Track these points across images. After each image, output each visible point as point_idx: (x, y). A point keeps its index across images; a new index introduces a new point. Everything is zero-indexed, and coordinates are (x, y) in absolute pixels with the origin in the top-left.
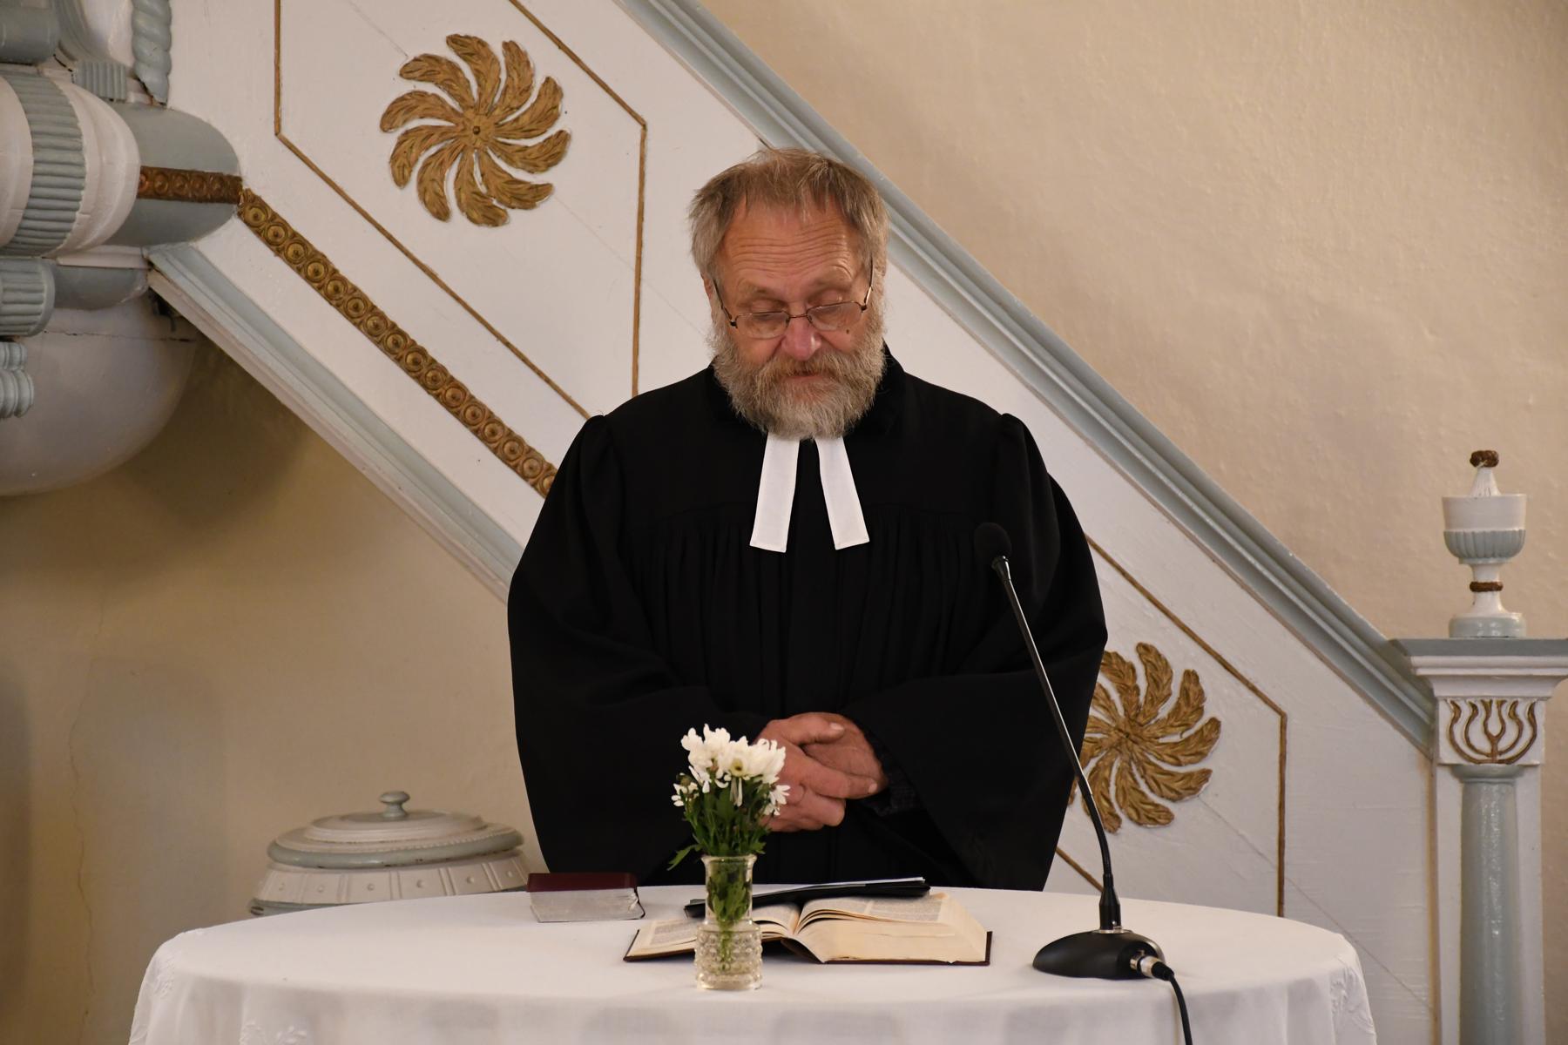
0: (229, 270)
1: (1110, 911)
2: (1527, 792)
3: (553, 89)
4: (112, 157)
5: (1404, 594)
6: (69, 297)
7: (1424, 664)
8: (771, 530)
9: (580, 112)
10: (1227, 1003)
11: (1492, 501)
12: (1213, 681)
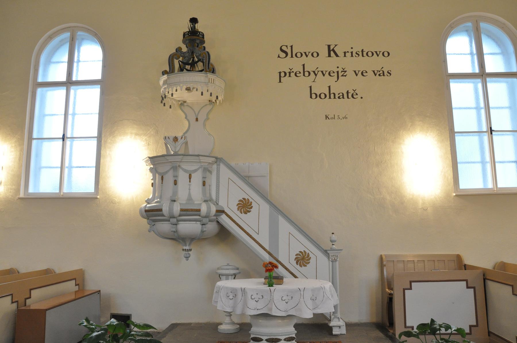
0: (223, 218)
2: (337, 262)
4: (214, 209)
5: (327, 245)
6: (210, 221)
7: (328, 252)
11: (334, 237)
12: (310, 253)
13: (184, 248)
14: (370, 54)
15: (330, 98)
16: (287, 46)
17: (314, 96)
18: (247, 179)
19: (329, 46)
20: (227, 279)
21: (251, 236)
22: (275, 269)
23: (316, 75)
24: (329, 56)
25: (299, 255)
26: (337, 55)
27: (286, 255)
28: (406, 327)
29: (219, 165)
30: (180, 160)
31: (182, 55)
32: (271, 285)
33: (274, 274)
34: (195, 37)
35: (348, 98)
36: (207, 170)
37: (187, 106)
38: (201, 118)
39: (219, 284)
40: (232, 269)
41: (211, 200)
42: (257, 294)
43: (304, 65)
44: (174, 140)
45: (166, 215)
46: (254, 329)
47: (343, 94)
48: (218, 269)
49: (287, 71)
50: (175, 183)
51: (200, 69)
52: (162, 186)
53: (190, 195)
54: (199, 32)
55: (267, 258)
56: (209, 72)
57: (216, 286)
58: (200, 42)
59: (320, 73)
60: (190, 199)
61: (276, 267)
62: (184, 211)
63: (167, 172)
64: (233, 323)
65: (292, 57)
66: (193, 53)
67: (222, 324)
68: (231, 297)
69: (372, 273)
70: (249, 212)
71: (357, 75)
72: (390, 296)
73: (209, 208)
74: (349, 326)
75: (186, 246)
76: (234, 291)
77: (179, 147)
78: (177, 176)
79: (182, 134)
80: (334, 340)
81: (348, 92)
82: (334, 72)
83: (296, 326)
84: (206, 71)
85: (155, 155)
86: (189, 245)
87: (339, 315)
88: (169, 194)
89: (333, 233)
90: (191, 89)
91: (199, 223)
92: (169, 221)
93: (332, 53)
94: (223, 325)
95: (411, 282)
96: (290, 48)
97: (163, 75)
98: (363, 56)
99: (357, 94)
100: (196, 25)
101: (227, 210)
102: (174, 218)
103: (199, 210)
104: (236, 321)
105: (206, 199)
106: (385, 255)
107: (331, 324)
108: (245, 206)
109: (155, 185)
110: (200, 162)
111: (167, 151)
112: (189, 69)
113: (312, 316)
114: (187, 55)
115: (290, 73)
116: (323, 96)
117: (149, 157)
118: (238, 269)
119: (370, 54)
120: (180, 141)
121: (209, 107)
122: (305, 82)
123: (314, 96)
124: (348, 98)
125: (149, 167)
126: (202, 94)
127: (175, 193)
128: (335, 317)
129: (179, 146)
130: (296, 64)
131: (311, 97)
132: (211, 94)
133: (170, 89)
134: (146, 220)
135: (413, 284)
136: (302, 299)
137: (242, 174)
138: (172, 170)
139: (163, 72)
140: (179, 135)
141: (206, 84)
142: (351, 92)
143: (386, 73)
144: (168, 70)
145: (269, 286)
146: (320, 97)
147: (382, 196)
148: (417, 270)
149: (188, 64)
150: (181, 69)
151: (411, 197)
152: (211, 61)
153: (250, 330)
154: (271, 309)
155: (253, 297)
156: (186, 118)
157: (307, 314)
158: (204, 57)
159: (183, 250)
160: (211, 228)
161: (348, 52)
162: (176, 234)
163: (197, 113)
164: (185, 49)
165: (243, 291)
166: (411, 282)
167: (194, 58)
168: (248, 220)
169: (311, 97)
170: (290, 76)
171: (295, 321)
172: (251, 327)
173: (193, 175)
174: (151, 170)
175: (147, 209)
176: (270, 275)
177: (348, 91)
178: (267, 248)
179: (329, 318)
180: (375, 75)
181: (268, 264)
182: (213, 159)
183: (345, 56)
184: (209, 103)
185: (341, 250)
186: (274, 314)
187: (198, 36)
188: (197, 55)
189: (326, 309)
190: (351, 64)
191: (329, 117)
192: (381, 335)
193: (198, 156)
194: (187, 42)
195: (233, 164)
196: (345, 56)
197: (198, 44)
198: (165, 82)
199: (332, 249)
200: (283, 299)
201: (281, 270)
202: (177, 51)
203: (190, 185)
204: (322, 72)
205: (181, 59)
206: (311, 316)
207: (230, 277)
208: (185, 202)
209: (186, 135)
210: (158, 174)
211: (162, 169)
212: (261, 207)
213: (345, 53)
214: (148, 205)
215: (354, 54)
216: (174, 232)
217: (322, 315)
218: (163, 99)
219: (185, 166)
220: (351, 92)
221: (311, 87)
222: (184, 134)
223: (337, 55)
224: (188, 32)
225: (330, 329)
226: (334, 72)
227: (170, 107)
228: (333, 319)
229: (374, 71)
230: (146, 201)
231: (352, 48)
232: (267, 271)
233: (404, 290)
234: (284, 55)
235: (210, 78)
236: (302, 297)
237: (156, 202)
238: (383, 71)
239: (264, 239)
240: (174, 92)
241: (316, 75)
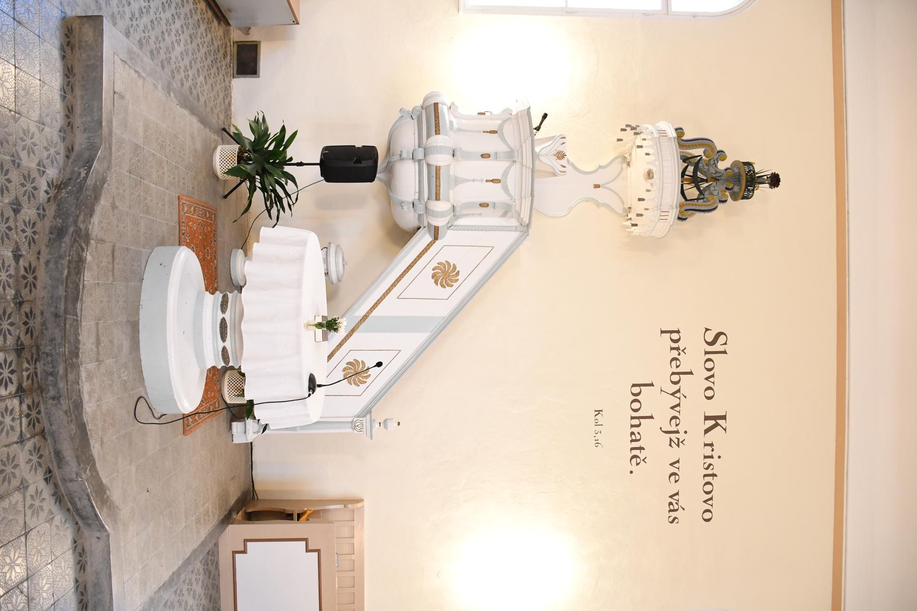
0: (423, 238)
1: (320, 386)
2: (351, 430)
3: (452, 286)
4: (440, 222)
5: (379, 415)
6: (420, 215)
7: (368, 416)
8: (266, 146)
9: (449, 290)
10: (305, 405)
11: (392, 425)
12: (366, 385)
14: (708, 488)
15: (632, 418)
16: (725, 344)
17: (636, 390)
19: (724, 417)
21: (394, 285)
23: (673, 394)
24: (707, 418)
29: (516, 230)
30: (525, 163)
31: (712, 162)
35: (632, 449)
36: (506, 211)
41: (456, 217)
43: (691, 373)
44: (559, 153)
49: (681, 345)
50: (485, 156)
52: (479, 132)
54: (753, 190)
56: (680, 212)
59: (677, 402)
60: (457, 181)
63: (503, 139)
65: (706, 353)
66: (716, 179)
70: (436, 282)
73: (442, 214)
81: (641, 448)
82: (677, 425)
84: (681, 206)
92: (419, 147)
93: (712, 422)
95: (318, 551)
96: (722, 349)
97: (676, 130)
98: (705, 476)
99: (638, 464)
103: (438, 199)
105: (458, 209)
108: (445, 275)
112: (687, 173)
114: (712, 170)
115: (678, 349)
116: (636, 405)
119: (708, 488)
120: (557, 164)
122: (662, 376)
123: (636, 390)
124: (632, 449)
126: (640, 200)
127: (468, 156)
130: (693, 359)
131: (634, 385)
132: (641, 215)
133: (650, 143)
138: (506, 149)
139: (681, 129)
142: (642, 455)
143: (673, 514)
146: (639, 394)
149: (695, 172)
150: (685, 159)
156: (600, 167)
158: (708, 201)
160: (408, 219)
164: (722, 166)
166: (318, 551)
167: (707, 181)
168: (421, 280)
169: (634, 385)
170: (672, 349)
174: (508, 111)
175: (440, 106)
180: (671, 497)
182: (526, 221)
183: (706, 445)
184: (626, 207)
188: (712, 188)
192: (232, 500)
193: (532, 195)
194: (736, 170)
196: (706, 445)
198: (662, 133)
199: (372, 421)
203: (482, 180)
204: (678, 405)
208: (451, 173)
212: (441, 303)
213: (711, 445)
215: (709, 461)
218: (633, 128)
219: (515, 169)
220: (642, 455)
221: (652, 385)
226: (677, 425)
229: (677, 494)
231: (719, 457)
233: (306, 540)
234: (710, 340)
237: (451, 122)
238: (677, 510)
240: (644, 150)
241: (673, 394)
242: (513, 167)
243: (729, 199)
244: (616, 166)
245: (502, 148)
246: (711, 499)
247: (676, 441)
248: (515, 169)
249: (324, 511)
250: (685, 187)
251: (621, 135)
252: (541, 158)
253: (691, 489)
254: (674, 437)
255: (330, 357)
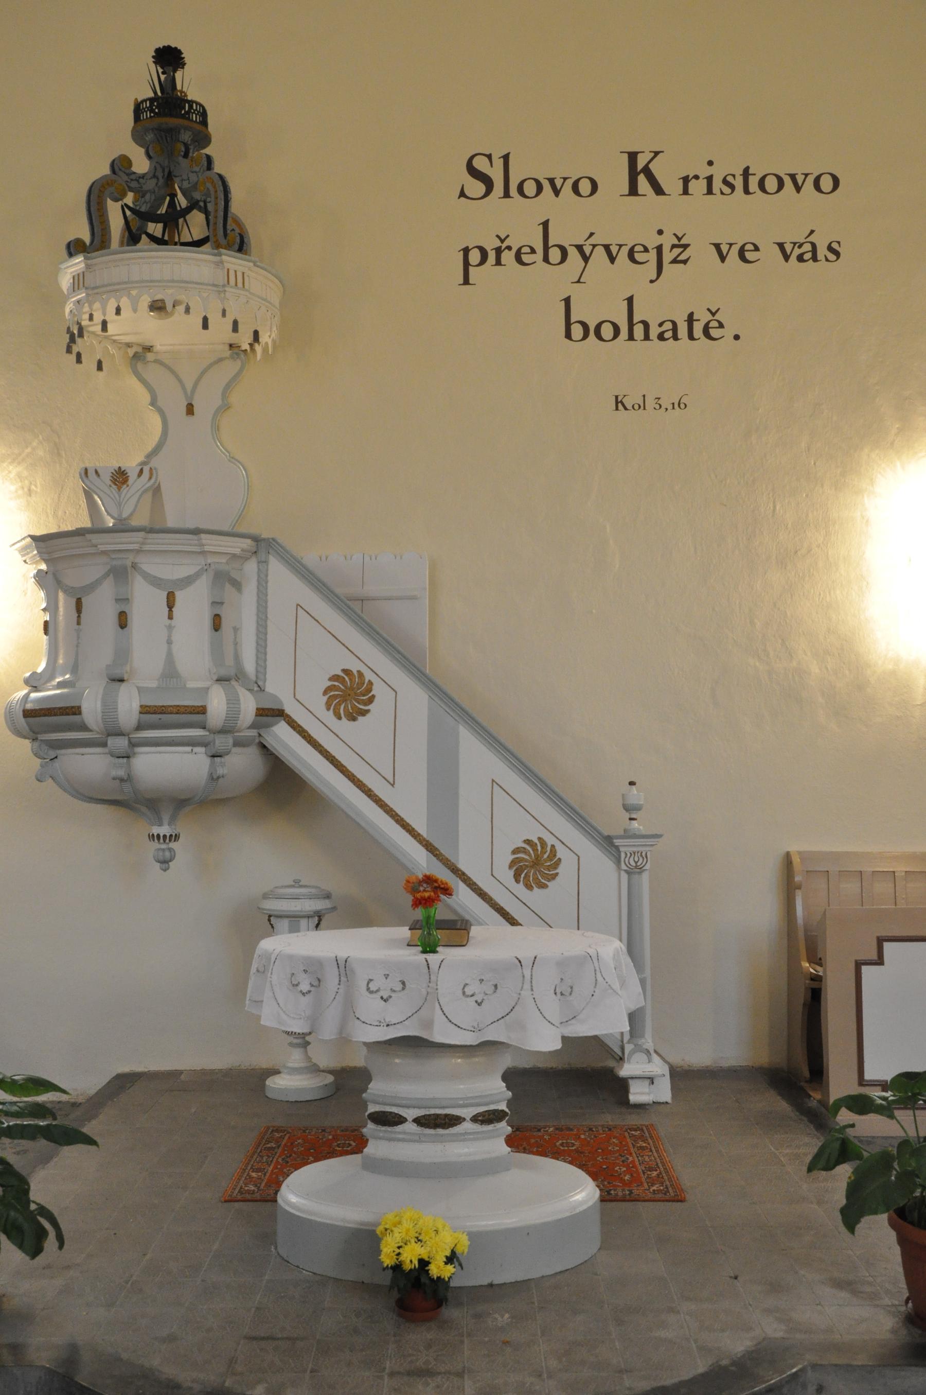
0: (282, 736)
2: (645, 876)
4: (248, 705)
5: (613, 821)
6: (238, 744)
7: (617, 842)
11: (635, 796)
12: (559, 848)
13: (156, 830)
14: (771, 184)
15: (631, 337)
16: (489, 157)
17: (577, 331)
18: (356, 606)
19: (633, 157)
20: (294, 929)
21: (369, 793)
22: (442, 897)
23: (586, 259)
24: (633, 191)
25: (524, 850)
26: (658, 190)
27: (482, 853)
28: (862, 1082)
29: (266, 562)
30: (135, 546)
31: (134, 184)
32: (429, 948)
33: (440, 912)
34: (173, 122)
35: (691, 337)
36: (225, 580)
37: (157, 361)
38: (205, 404)
39: (268, 945)
40: (311, 897)
41: (239, 675)
42: (387, 976)
43: (545, 225)
44: (114, 481)
45: (94, 727)
46: (376, 1087)
47: (674, 324)
48: (265, 896)
49: (491, 244)
50: (123, 621)
51: (197, 235)
52: (78, 632)
53: (170, 659)
54: (191, 103)
55: (421, 862)
56: (229, 247)
57: (258, 952)
58: (194, 141)
59: (600, 251)
60: (170, 673)
61: (447, 891)
62: (154, 715)
63: (91, 587)
64: (315, 1069)
65: (507, 195)
66: (170, 178)
67: (277, 1072)
68: (305, 987)
69: (755, 912)
70: (364, 713)
71: (723, 258)
72: (815, 985)
73: (233, 702)
74: (681, 1076)
75: (161, 825)
76: (313, 968)
77: (133, 503)
78: (126, 600)
79: (140, 458)
80: (633, 1120)
81: (691, 319)
82: (646, 250)
83: (510, 1077)
84: (218, 246)
85: (53, 530)
86: (173, 820)
87: (648, 1042)
88: (101, 657)
89: (632, 783)
90: (169, 307)
91: (201, 750)
92: (104, 745)
93: (642, 179)
94: (282, 1075)
95: (880, 941)
96: (499, 163)
97: (71, 255)
98: (747, 191)
99: (721, 326)
100: (178, 75)
101: (291, 709)
102: (121, 734)
103: (202, 710)
104: (324, 1060)
105: (223, 672)
106: (799, 853)
107: (625, 1071)
108: (350, 696)
109: (56, 630)
110: (203, 553)
111: (91, 516)
112: (158, 234)
113: (557, 1045)
114: (151, 184)
115: (499, 251)
116: (607, 332)
117: (33, 538)
118: (328, 896)
119: (771, 184)
120: (136, 485)
121: (231, 368)
122: (549, 281)
123: (577, 331)
124: (691, 337)
125: (32, 570)
126: (205, 325)
127: (123, 654)
128: (638, 1049)
129: (134, 500)
130: (517, 220)
131: (568, 335)
132: (235, 324)
133: (97, 305)
134: (27, 743)
135: (887, 946)
136: (526, 993)
137: (338, 591)
138: (110, 580)
139: (69, 246)
140: (131, 463)
141: (220, 289)
142: (703, 317)
143: (822, 252)
144: (87, 239)
145: (424, 952)
146: (599, 336)
147: (794, 664)
148: (902, 905)
149: (156, 219)
150: (132, 237)
151: (890, 667)
152: (234, 208)
153: (365, 1090)
154: (428, 1024)
155: (373, 987)
156: (153, 403)
157: (543, 1040)
158: (208, 194)
159: (152, 837)
160: (243, 765)
161: (696, 177)
162: (127, 787)
163: (189, 387)
164: (141, 165)
165: (344, 967)
166: (880, 941)
167: (173, 196)
168: (360, 741)
169: (568, 335)
170: (498, 262)
171: (507, 1061)
172: (371, 1081)
173: (179, 596)
174: (40, 578)
175: (29, 706)
176: (428, 918)
177: (691, 315)
178: (422, 830)
179: (618, 1050)
180: (787, 257)
181: (420, 883)
182: (247, 543)
183: (686, 192)
184: (228, 353)
185: (659, 836)
186: (438, 1038)
187: (186, 116)
188: (186, 185)
189: (606, 1021)
190: (708, 219)
191: (628, 402)
192: (783, 1106)
193: (196, 532)
194: (150, 137)
195: (310, 558)
196: (686, 192)
197: (186, 145)
198: (78, 282)
199: (628, 835)
200: (469, 991)
201: (463, 900)
202: (113, 171)
203: (170, 628)
204: (607, 248)
205: (129, 199)
206: (556, 1045)
207: (303, 922)
208: (154, 684)
209: (154, 463)
210: (65, 592)
211: (78, 576)
212: (401, 701)
213: (686, 180)
214: (34, 695)
215: (717, 184)
216: (122, 780)
217: (596, 1040)
218: (72, 340)
219: (151, 566)
220: (703, 317)
221: (567, 301)
222: (150, 456)
223: (658, 190)
224: (151, 100)
225: (623, 1085)
226: (646, 250)
227: (100, 367)
228: (632, 1052)
229: (781, 246)
230: (27, 682)
231: (710, 163)
232: (417, 903)
233: (858, 965)
234: (480, 188)
235: (232, 268)
236: (527, 986)
237: (60, 685)
238: (814, 245)
239: (414, 805)
240: (111, 316)
241: (586, 259)
242: (145, 567)
243: (207, 151)
244: (153, 373)
245: (107, 591)
246: (793, 177)
247: (677, 251)
248: (151, 566)
249: (806, 931)
250: (186, 238)
251: (89, 363)
252: (124, 515)
253: (766, 219)
254: (669, 254)
255: (513, 922)
